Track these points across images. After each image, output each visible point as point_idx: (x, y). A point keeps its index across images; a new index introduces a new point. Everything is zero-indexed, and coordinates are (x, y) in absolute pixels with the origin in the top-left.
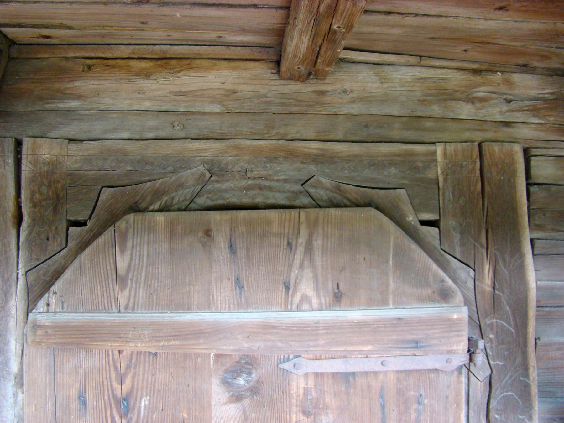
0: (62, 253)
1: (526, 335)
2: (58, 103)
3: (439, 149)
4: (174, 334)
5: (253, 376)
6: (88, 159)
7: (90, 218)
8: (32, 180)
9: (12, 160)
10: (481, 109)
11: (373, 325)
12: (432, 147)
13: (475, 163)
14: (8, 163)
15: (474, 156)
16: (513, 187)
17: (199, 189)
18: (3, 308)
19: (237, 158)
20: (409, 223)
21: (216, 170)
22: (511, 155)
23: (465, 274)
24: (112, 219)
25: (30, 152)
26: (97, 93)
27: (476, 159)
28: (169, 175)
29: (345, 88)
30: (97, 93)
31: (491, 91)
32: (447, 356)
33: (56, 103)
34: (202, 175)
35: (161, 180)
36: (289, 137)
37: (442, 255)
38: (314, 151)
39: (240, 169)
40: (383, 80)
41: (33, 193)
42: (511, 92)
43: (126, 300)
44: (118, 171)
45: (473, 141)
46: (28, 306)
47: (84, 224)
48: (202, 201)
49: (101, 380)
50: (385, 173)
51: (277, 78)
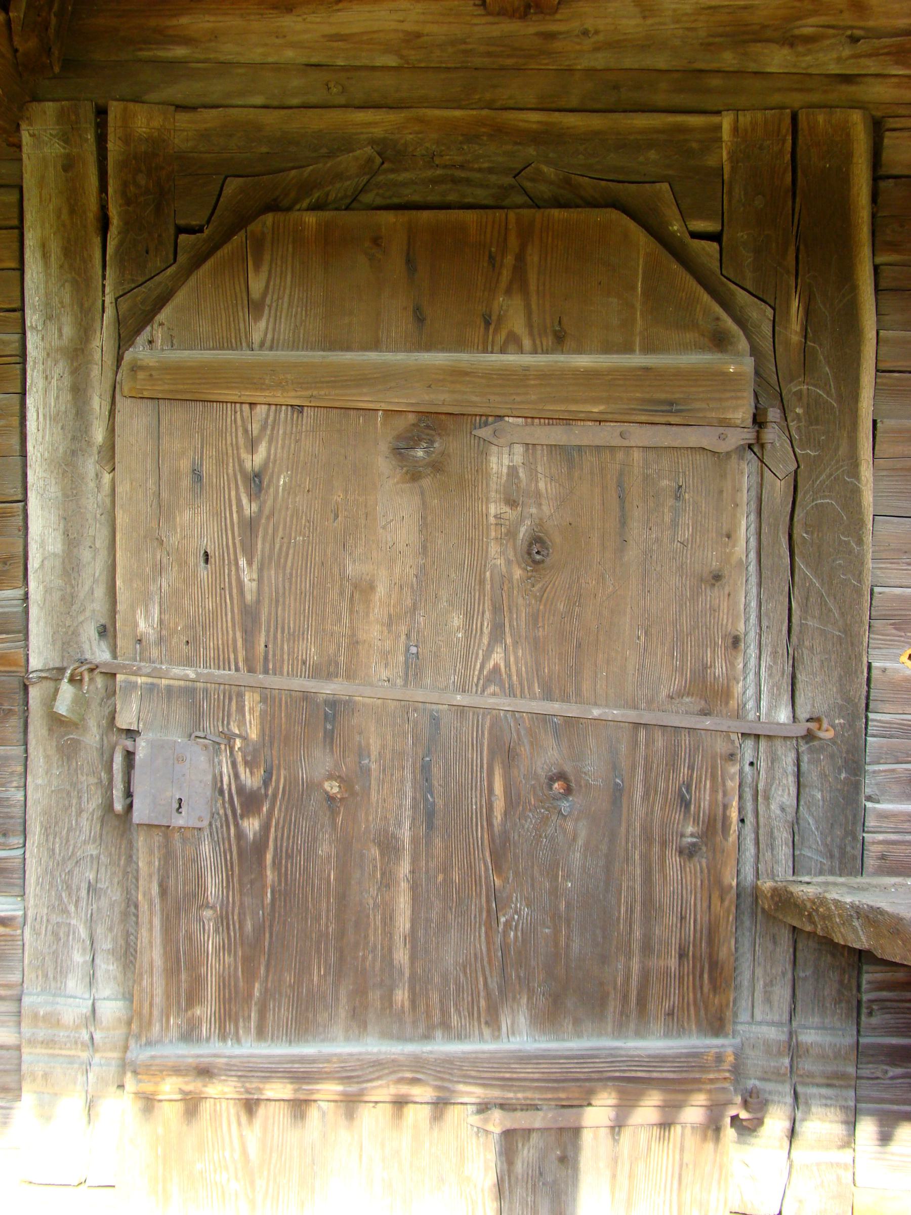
1: (857, 411)
2: (156, 49)
3: (726, 122)
4: (328, 379)
5: (436, 445)
6: (205, 136)
7: (208, 222)
8: (124, 164)
9: (93, 135)
10: (804, 55)
12: (715, 119)
13: (784, 141)
15: (784, 131)
16: (844, 179)
17: (365, 181)
18: (83, 350)
19: (420, 136)
20: (673, 234)
21: (390, 153)
22: (845, 132)
23: (760, 315)
24: (241, 221)
25: (119, 123)
26: (214, 36)
27: (786, 136)
29: (586, 26)
30: (214, 36)
31: (827, 24)
32: (721, 430)
34: (370, 160)
35: (311, 167)
37: (723, 284)
38: (534, 126)
39: (424, 152)
40: (647, 13)
41: (125, 184)
42: (862, 24)
46: (119, 348)
47: (200, 230)
49: (224, 447)
50: (641, 159)
51: (483, 12)
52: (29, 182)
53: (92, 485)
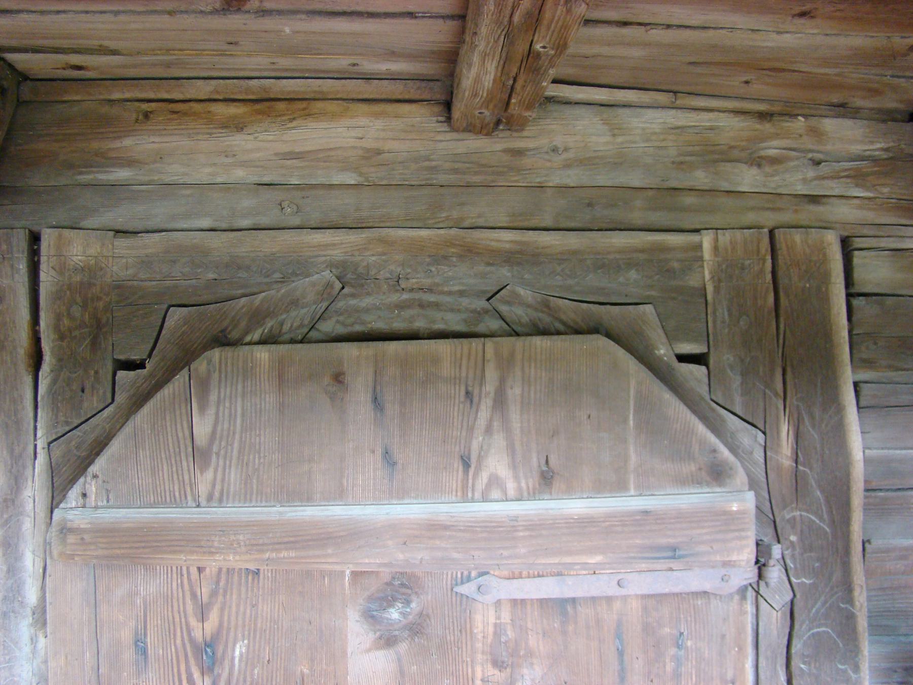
0: (106, 413)
1: (848, 536)
2: (98, 172)
3: (707, 240)
5: (413, 605)
6: (146, 263)
7: (150, 356)
8: (57, 296)
9: (25, 265)
10: (772, 176)
13: (764, 261)
14: (18, 270)
15: (763, 251)
16: (825, 299)
18: (13, 501)
20: (660, 358)
21: (350, 277)
22: (821, 248)
23: (750, 439)
24: (185, 358)
25: (52, 252)
26: (160, 157)
27: (765, 255)
28: (275, 286)
29: (554, 143)
30: (160, 157)
32: (723, 571)
33: (93, 172)
34: (329, 285)
35: (263, 294)
36: (467, 224)
37: (713, 410)
38: (507, 246)
39: (388, 275)
40: (616, 131)
41: (58, 317)
42: (820, 148)
44: (194, 281)
47: (141, 365)
48: (328, 327)
49: (170, 614)
50: (621, 279)
53: (27, 649)
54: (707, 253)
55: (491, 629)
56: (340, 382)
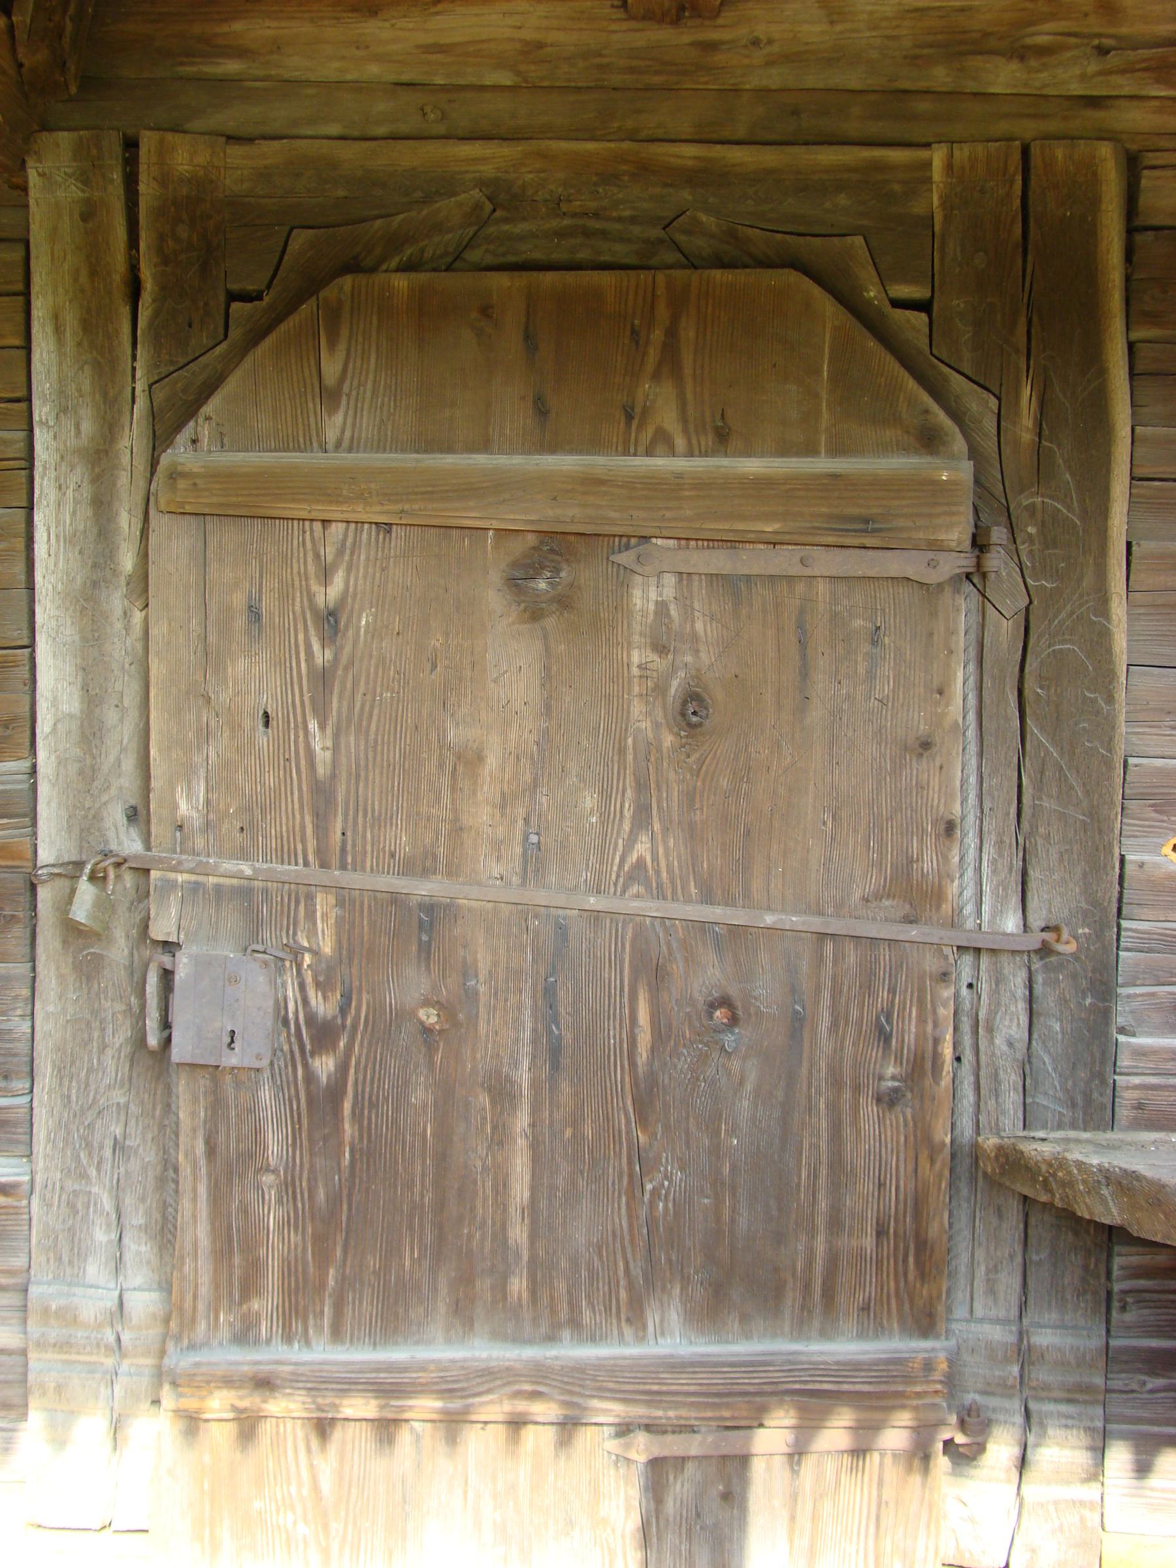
0: (218, 350)
1: (1106, 531)
3: (937, 157)
4: (423, 489)
5: (563, 574)
7: (269, 287)
9: (120, 174)
10: (1038, 71)
11: (784, 484)
12: (923, 154)
14: (112, 180)
15: (1012, 169)
16: (1090, 232)
17: (471, 233)
18: (107, 452)
19: (542, 175)
20: (869, 302)
21: (503, 197)
23: (981, 406)
27: (1014, 175)
30: (277, 46)
31: (1067, 30)
32: (931, 555)
34: (478, 206)
35: (402, 216)
36: (643, 135)
37: (934, 367)
38: (690, 163)
40: (835, 17)
41: (161, 238)
42: (1112, 31)
43: (338, 431)
45: (1011, 139)
46: (154, 448)
47: (259, 297)
48: (474, 256)
49: (289, 577)
50: (828, 205)
51: (623, 16)
52: (38, 235)
53: (119, 625)
54: (937, 173)
55: (652, 607)
56: (489, 317)
